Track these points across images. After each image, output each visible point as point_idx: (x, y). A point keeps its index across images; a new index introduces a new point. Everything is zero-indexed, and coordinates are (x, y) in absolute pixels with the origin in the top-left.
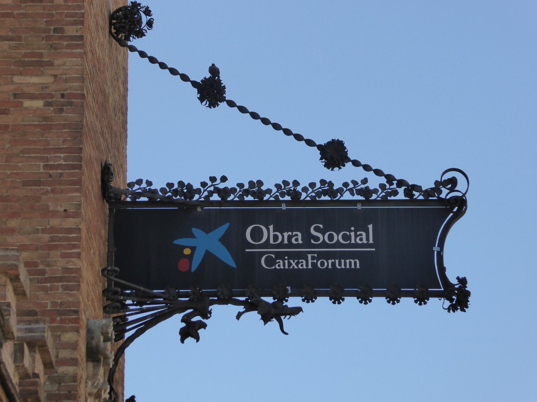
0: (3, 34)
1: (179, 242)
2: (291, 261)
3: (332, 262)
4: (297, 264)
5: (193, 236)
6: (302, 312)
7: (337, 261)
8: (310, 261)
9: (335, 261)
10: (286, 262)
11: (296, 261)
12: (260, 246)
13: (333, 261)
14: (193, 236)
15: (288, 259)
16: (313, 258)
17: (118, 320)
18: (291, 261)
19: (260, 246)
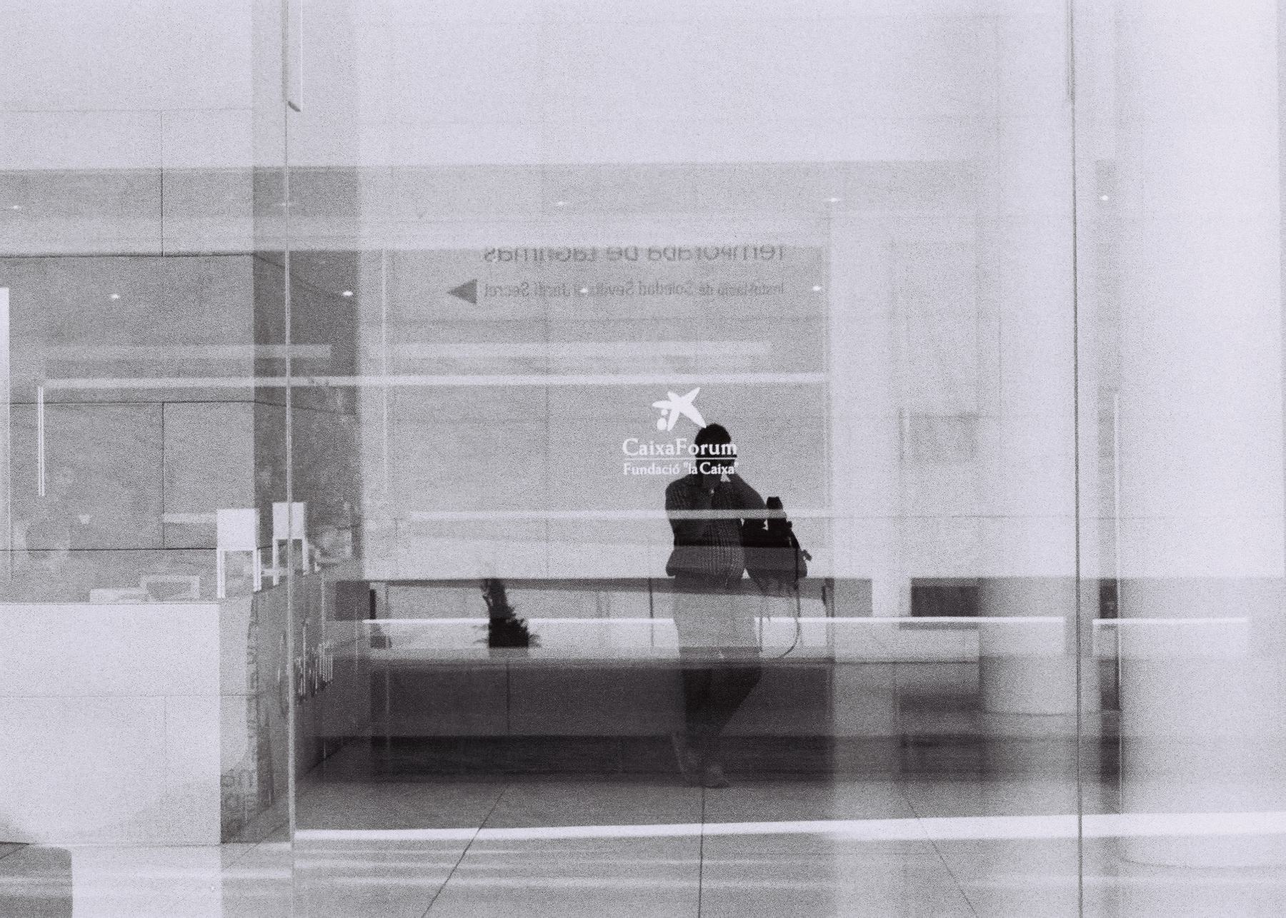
0: (1078, 917)
1: (656, 405)
2: (723, 468)
3: (706, 448)
4: (664, 450)
5: (667, 399)
6: (663, 574)
7: (711, 446)
8: (679, 446)
9: (708, 447)
10: (719, 468)
11: (662, 446)
12: (705, 461)
13: (706, 446)
14: (667, 399)
15: (721, 466)
16: (682, 443)
17: (318, 407)
18: (657, 446)
19: (705, 461)
